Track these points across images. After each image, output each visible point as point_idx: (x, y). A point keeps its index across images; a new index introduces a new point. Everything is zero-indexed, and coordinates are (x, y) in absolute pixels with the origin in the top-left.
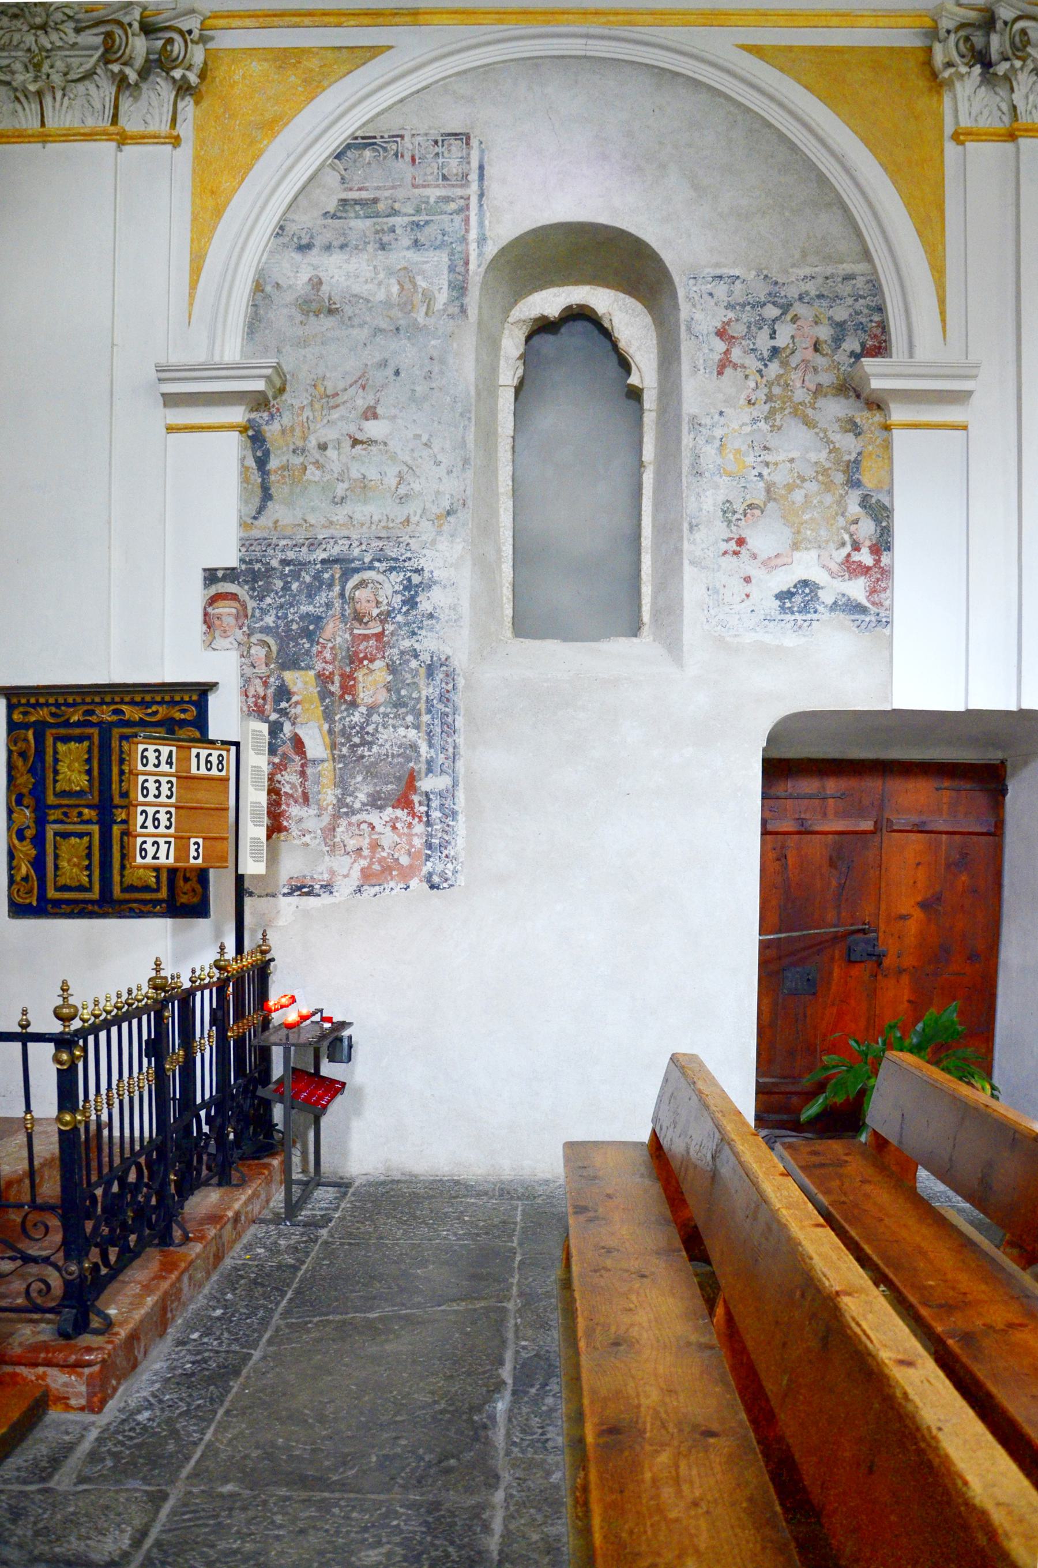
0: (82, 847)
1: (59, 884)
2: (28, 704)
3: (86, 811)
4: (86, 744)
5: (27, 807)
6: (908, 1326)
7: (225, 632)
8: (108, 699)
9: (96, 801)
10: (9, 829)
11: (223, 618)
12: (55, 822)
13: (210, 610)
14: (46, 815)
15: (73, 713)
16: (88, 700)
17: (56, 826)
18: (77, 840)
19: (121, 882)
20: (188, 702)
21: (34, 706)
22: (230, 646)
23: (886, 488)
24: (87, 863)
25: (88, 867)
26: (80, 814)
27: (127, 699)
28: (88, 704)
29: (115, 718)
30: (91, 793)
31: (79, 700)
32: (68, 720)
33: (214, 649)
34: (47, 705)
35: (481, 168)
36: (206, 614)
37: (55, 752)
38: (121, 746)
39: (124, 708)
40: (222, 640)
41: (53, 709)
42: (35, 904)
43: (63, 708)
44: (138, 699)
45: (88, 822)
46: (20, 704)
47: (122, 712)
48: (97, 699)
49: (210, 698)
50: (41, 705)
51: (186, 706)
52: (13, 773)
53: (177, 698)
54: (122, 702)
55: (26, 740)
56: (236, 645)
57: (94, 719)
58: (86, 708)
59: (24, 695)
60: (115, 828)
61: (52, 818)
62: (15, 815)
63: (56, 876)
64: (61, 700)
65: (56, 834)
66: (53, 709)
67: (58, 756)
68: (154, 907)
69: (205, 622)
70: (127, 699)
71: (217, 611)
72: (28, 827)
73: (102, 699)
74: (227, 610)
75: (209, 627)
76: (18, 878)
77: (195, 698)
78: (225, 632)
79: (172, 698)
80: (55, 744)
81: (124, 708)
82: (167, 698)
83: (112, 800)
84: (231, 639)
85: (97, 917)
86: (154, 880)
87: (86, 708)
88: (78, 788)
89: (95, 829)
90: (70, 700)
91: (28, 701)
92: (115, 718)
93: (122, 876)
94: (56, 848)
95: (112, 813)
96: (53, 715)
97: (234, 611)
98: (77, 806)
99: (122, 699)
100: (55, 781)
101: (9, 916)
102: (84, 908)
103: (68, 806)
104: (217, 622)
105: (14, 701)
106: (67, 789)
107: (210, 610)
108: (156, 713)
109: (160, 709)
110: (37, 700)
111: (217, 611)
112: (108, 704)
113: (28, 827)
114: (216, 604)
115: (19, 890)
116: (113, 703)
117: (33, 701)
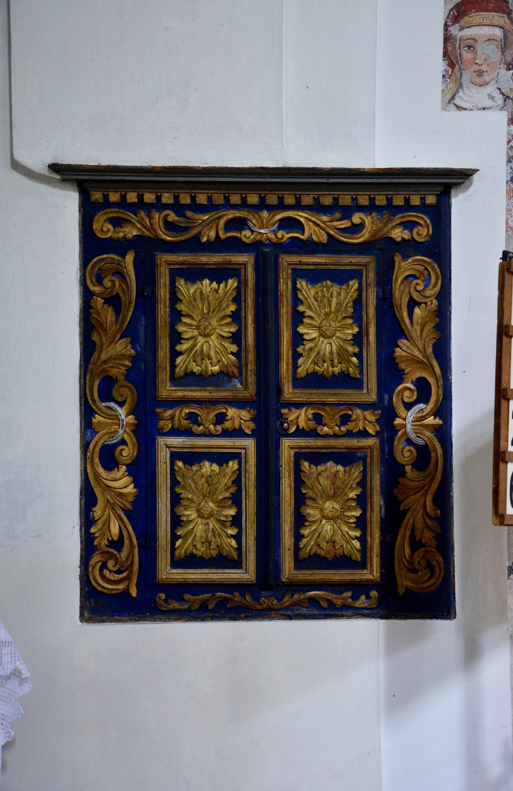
0: (226, 481)
1: (180, 553)
2: (123, 204)
3: (231, 412)
4: (232, 283)
5: (121, 404)
6: (90, 166)
7: (480, 73)
8: (272, 199)
9: (251, 391)
10: (85, 446)
11: (479, 47)
12: (175, 432)
13: (454, 30)
14: (157, 417)
15: (206, 224)
16: (235, 199)
17: (176, 441)
18: (215, 467)
19: (297, 549)
20: (415, 208)
21: (134, 208)
22: (489, 103)
23: (96, 559)
24: (232, 512)
25: (236, 521)
26: (221, 418)
27: (307, 200)
28: (235, 207)
29: (285, 235)
30: (241, 376)
31: (218, 199)
32: (198, 237)
33: (459, 108)
34: (159, 206)
35: (425, 368)
36: (447, 39)
37: (174, 299)
38: (295, 289)
39: (301, 216)
40: (474, 89)
41: (172, 217)
42: (134, 593)
43: (189, 214)
44: (327, 201)
45: (239, 433)
46: (106, 204)
47: (300, 227)
48: (253, 199)
49: (454, 201)
50: (148, 208)
51: (412, 216)
52: (95, 338)
53: (398, 201)
54: (298, 206)
55: (121, 275)
56: (499, 99)
57: (246, 236)
58: (231, 214)
59: (115, 185)
60: (286, 443)
61: (166, 425)
62: (97, 419)
63: (174, 537)
64: (185, 199)
65: (175, 456)
66: (172, 217)
67: (180, 307)
68: (355, 598)
69: (446, 54)
70: (307, 200)
71: (467, 32)
72: (123, 442)
73: (262, 199)
74: (486, 31)
75: (452, 65)
76: (101, 542)
77: (431, 200)
78: (480, 73)
79: (389, 200)
80: (173, 282)
81: (301, 216)
82: (381, 200)
83: (280, 391)
84: (491, 89)
85: (248, 618)
86: (357, 544)
87: (231, 214)
88: (216, 369)
89: (250, 444)
90: (202, 199)
91: (123, 197)
92: (285, 235)
93: (298, 537)
94: (174, 483)
95: (281, 417)
96: (169, 226)
97: (498, 32)
98: (213, 402)
99: (298, 200)
100: (175, 354)
101: (82, 618)
102: (225, 600)
103: (199, 402)
104: (467, 55)
105: (97, 196)
106: (196, 369)
107: (454, 30)
108: (357, 228)
109: (368, 220)
110: (140, 197)
111: (467, 32)
112: (271, 208)
113: (123, 442)
114: (462, 22)
115: (104, 566)
116: (282, 206)
117: (132, 197)
